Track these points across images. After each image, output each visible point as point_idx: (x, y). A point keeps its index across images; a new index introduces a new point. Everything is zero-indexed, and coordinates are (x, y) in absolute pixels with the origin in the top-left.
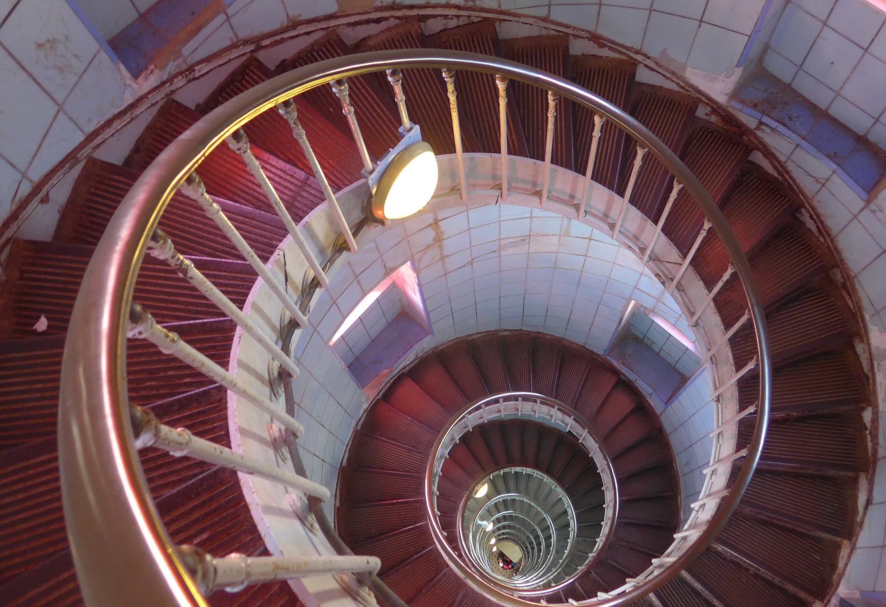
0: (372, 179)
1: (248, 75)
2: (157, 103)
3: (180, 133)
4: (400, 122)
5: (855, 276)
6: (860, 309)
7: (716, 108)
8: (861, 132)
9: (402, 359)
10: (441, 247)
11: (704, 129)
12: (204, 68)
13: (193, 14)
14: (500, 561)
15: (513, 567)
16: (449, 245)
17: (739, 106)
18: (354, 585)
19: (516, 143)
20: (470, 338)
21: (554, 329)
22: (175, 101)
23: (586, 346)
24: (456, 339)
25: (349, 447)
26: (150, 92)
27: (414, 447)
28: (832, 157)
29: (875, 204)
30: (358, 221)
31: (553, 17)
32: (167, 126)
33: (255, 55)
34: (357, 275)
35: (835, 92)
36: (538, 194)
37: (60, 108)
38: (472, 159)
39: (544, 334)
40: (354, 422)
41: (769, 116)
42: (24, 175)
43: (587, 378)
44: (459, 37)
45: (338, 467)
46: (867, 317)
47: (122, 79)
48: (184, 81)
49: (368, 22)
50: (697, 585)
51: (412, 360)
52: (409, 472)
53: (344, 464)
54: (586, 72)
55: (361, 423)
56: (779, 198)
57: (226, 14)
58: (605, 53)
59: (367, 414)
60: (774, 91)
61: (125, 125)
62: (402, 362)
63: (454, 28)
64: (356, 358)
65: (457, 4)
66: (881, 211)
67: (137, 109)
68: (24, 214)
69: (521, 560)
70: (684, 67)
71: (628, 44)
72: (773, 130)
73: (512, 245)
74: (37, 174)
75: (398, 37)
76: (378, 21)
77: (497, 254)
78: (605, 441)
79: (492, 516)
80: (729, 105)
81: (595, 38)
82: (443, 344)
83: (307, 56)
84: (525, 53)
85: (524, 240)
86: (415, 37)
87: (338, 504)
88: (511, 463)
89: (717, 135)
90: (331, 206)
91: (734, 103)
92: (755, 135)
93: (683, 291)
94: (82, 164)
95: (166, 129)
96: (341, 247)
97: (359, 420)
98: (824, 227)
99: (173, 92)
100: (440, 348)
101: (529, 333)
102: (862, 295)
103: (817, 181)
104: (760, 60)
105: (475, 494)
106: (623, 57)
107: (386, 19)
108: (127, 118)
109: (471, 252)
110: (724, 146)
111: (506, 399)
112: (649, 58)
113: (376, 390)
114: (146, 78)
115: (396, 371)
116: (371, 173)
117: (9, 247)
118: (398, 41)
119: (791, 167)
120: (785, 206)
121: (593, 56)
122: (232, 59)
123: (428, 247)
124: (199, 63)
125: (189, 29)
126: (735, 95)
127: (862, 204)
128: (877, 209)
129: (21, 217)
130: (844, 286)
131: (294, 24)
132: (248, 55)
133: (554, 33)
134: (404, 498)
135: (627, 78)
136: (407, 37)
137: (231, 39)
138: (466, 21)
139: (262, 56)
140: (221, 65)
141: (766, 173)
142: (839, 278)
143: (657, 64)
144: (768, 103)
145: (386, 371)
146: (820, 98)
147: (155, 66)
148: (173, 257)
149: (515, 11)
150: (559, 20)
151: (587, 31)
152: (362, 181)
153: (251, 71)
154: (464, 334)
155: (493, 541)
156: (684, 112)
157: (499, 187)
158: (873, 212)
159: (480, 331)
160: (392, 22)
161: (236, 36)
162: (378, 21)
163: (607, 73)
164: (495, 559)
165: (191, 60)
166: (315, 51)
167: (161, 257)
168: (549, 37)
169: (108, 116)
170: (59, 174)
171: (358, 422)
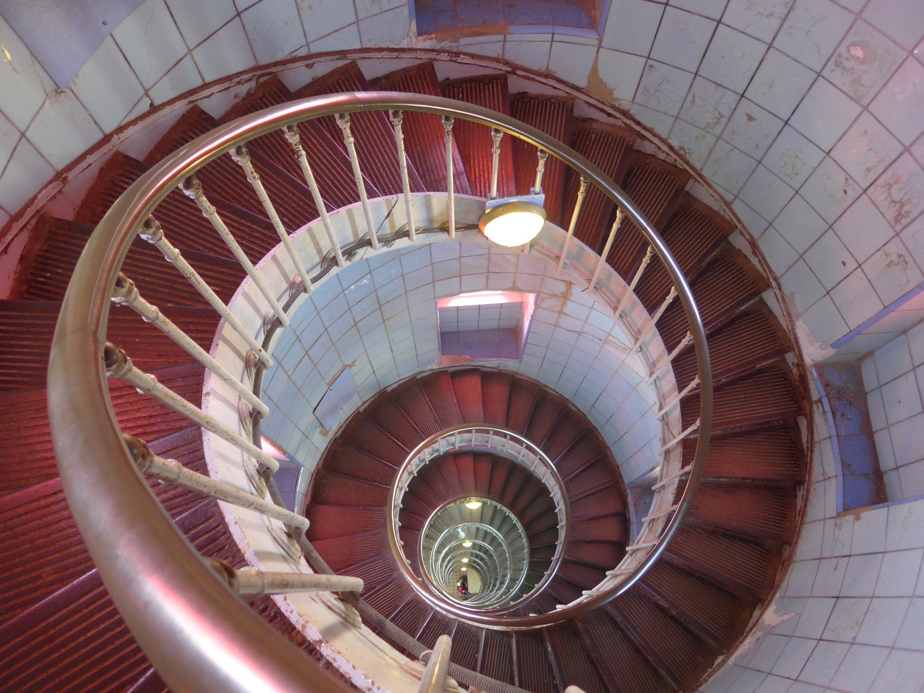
0: (490, 203)
1: (493, 84)
2: (421, 59)
3: (358, 90)
4: (533, 185)
5: (794, 562)
6: (778, 586)
7: (801, 364)
8: (883, 469)
9: (484, 359)
10: (564, 304)
11: (783, 372)
12: (467, 60)
13: (485, 22)
14: (461, 581)
15: (465, 594)
16: (570, 307)
17: (815, 375)
18: (252, 362)
19: (627, 264)
20: (547, 389)
21: (608, 435)
22: (433, 66)
23: (620, 468)
24: (536, 380)
25: (401, 382)
26: (421, 50)
27: (441, 421)
28: (846, 466)
29: (841, 520)
30: (472, 223)
31: (734, 206)
32: (416, 77)
33: (508, 74)
34: (490, 271)
35: (888, 424)
36: (615, 309)
37: (357, 22)
38: (582, 248)
39: (599, 433)
40: (418, 370)
41: (829, 401)
42: (307, 44)
43: (601, 490)
44: (658, 168)
45: (382, 388)
46: (777, 595)
47: (408, 30)
48: (449, 58)
49: (602, 110)
50: (515, 656)
51: (493, 366)
52: (423, 433)
53: (389, 390)
54: (730, 263)
55: (422, 375)
56: (792, 464)
57: (505, 37)
58: (755, 261)
59: (432, 373)
60: (852, 388)
61: (391, 58)
62: (483, 361)
63: (661, 160)
64: (458, 332)
65: (673, 145)
66: (840, 529)
67: (405, 54)
68: (290, 65)
69: (475, 594)
70: (799, 316)
71: (773, 267)
72: (824, 412)
73: (615, 345)
74: (315, 48)
75: (615, 136)
76: (609, 115)
77: (601, 343)
78: (571, 544)
79: (476, 539)
80: (810, 369)
81: (754, 245)
82: (523, 375)
83: (543, 102)
84: (697, 215)
85: (626, 350)
86: (625, 144)
87: (361, 410)
88: (511, 507)
89: (788, 384)
90: (449, 198)
91: (814, 371)
92: (811, 406)
93: (668, 462)
94: (347, 62)
95: (413, 78)
96: (444, 229)
97: (423, 372)
98: (804, 510)
99: (435, 59)
100: (519, 377)
101: (589, 423)
102: (787, 577)
103: (823, 474)
104: (861, 359)
105: (467, 503)
106: (765, 275)
107: (616, 118)
108: (395, 55)
109: (583, 327)
110: (785, 395)
111: (528, 448)
112: (780, 289)
113: (451, 363)
114: (425, 40)
115: (475, 364)
116: (492, 199)
117: (269, 77)
118: (613, 138)
119: (816, 449)
120: (791, 473)
121: (745, 256)
122: (490, 67)
123: (555, 296)
124: (466, 54)
125: (474, 29)
126: (819, 366)
127: (834, 514)
128: (839, 524)
129: (287, 66)
130: (784, 562)
131: (548, 75)
132: (504, 72)
133: (729, 219)
134: (404, 445)
135: (754, 289)
136: (620, 141)
137: (499, 55)
138: (672, 162)
139: (512, 79)
140: (480, 66)
141: (800, 440)
142: (786, 554)
143: (783, 298)
144: (839, 392)
145: (468, 357)
146: (877, 422)
147: (436, 37)
148: (295, 145)
149: (710, 182)
150: (737, 212)
151: (750, 235)
152: (483, 199)
153: (497, 83)
154: (543, 382)
155: (465, 560)
156: (776, 347)
157: (589, 281)
158: (836, 525)
159: (556, 390)
160: (619, 123)
161: (503, 55)
162: (609, 115)
163: (744, 275)
164: (458, 577)
165: (461, 49)
166: (550, 101)
167: (290, 141)
168: (723, 219)
169: (384, 45)
170: (328, 57)
171: (421, 372)
